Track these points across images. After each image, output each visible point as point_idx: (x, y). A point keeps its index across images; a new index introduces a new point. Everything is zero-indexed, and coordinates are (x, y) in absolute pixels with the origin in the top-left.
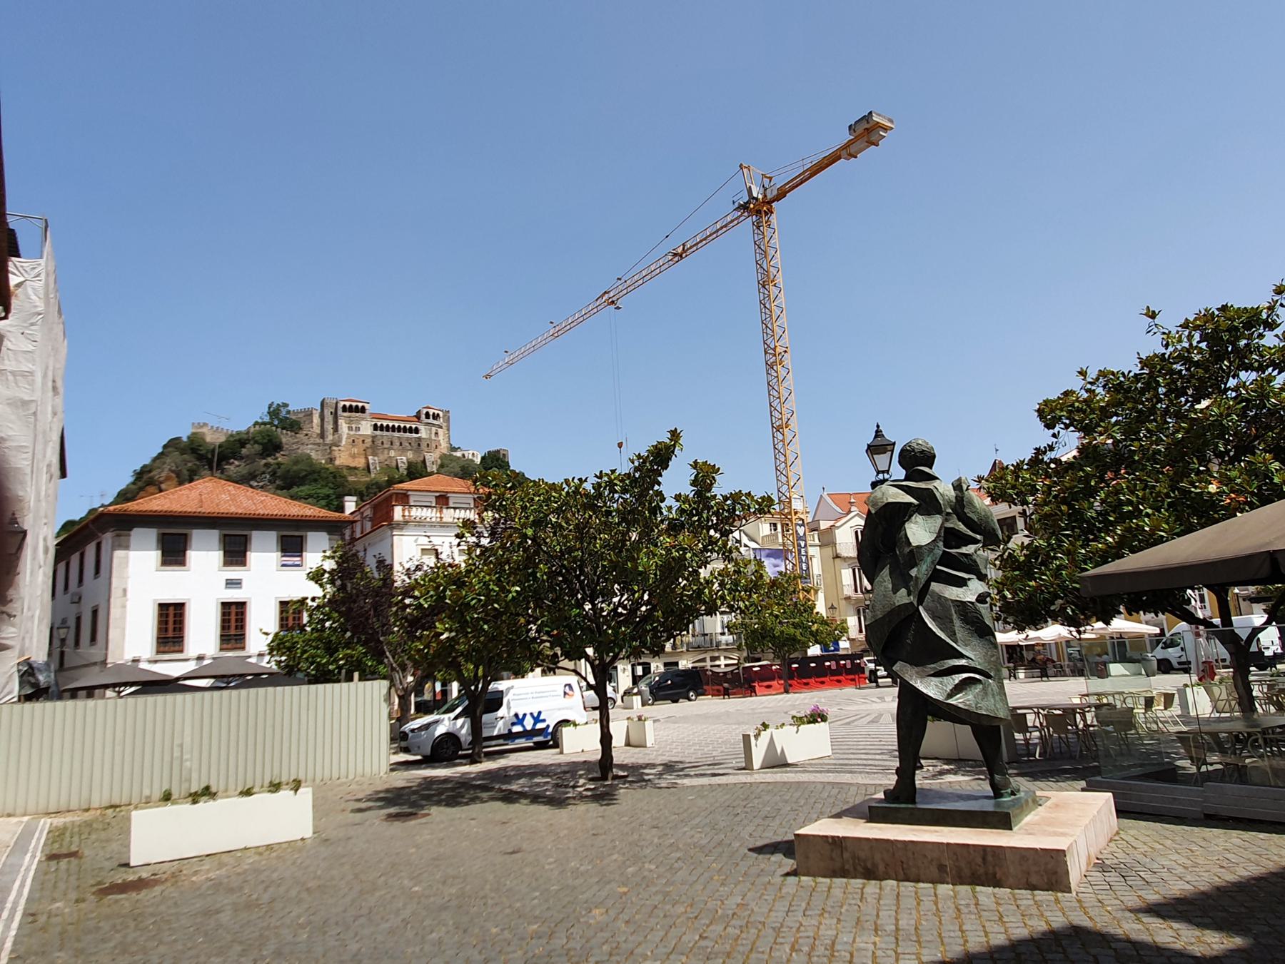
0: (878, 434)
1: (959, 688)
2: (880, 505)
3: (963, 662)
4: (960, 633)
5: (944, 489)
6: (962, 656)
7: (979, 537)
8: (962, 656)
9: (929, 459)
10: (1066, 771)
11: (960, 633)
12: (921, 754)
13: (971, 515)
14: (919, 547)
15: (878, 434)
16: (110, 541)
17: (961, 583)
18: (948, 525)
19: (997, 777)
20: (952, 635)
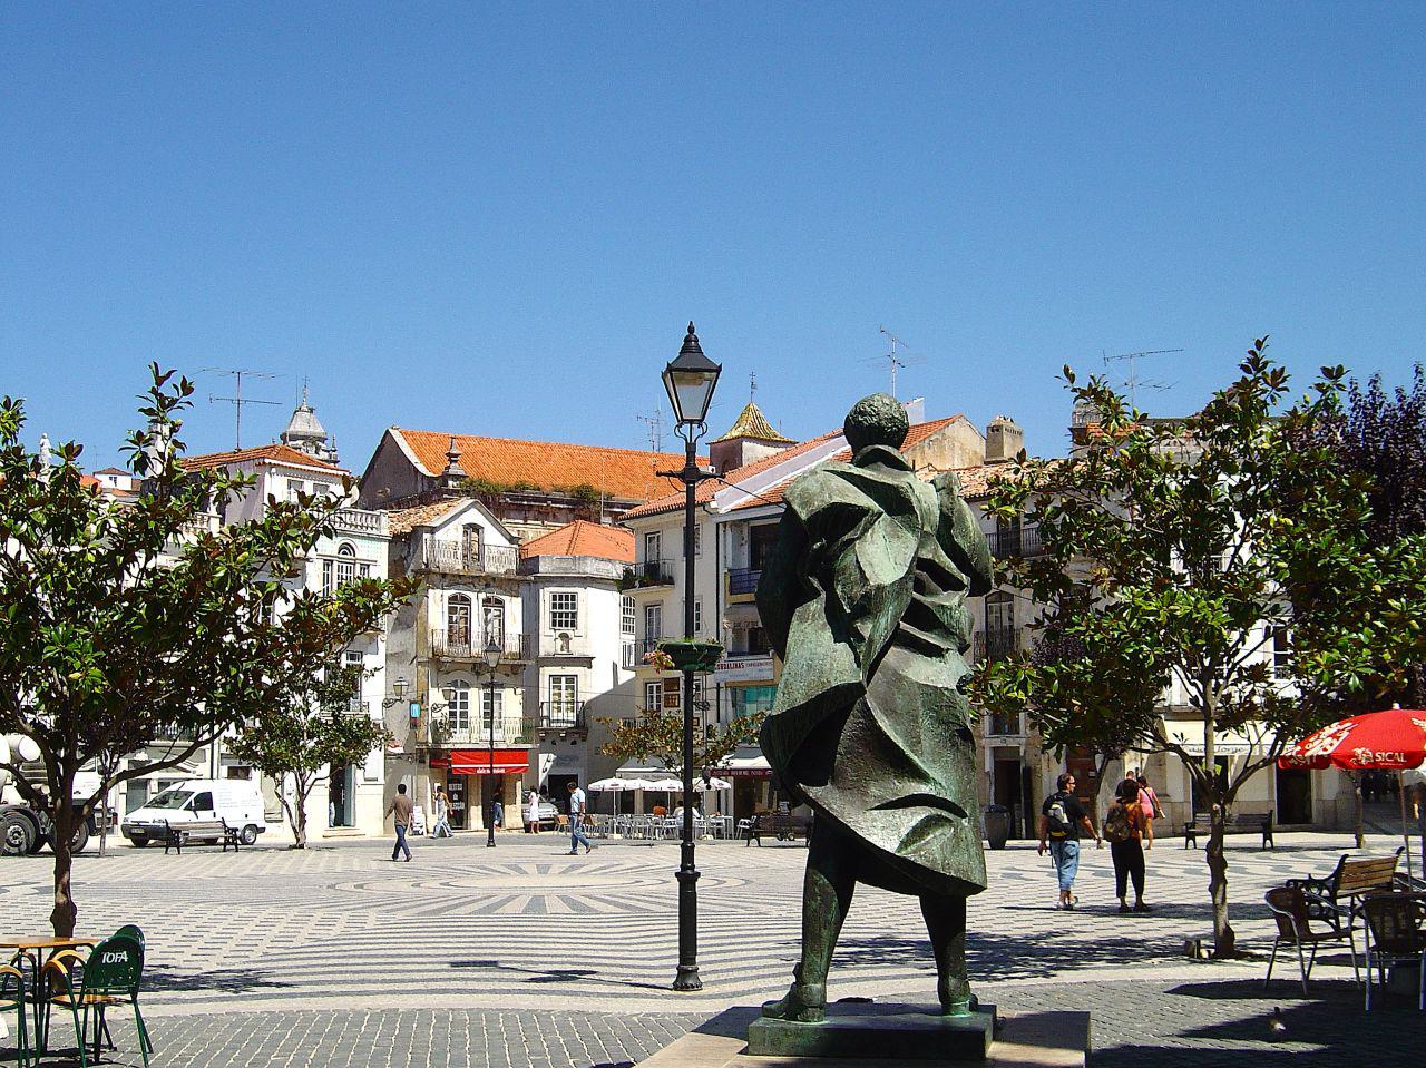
0: (690, 345)
1: (918, 832)
2: (817, 505)
3: (924, 789)
4: (927, 742)
5: (922, 491)
6: (921, 776)
7: (965, 579)
8: (921, 776)
9: (897, 432)
10: (1163, 907)
11: (927, 742)
12: (937, 978)
13: (958, 540)
14: (880, 588)
15: (690, 345)
16: (882, 533)
17: (937, 652)
18: (926, 554)
19: (952, 982)
20: (915, 742)
